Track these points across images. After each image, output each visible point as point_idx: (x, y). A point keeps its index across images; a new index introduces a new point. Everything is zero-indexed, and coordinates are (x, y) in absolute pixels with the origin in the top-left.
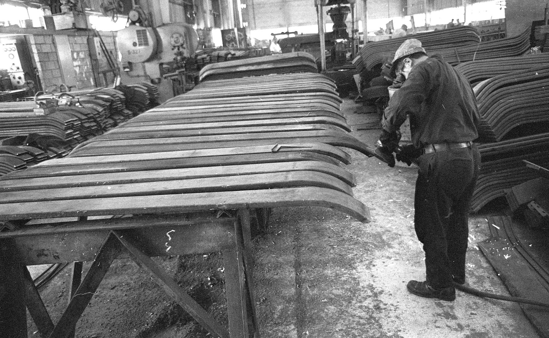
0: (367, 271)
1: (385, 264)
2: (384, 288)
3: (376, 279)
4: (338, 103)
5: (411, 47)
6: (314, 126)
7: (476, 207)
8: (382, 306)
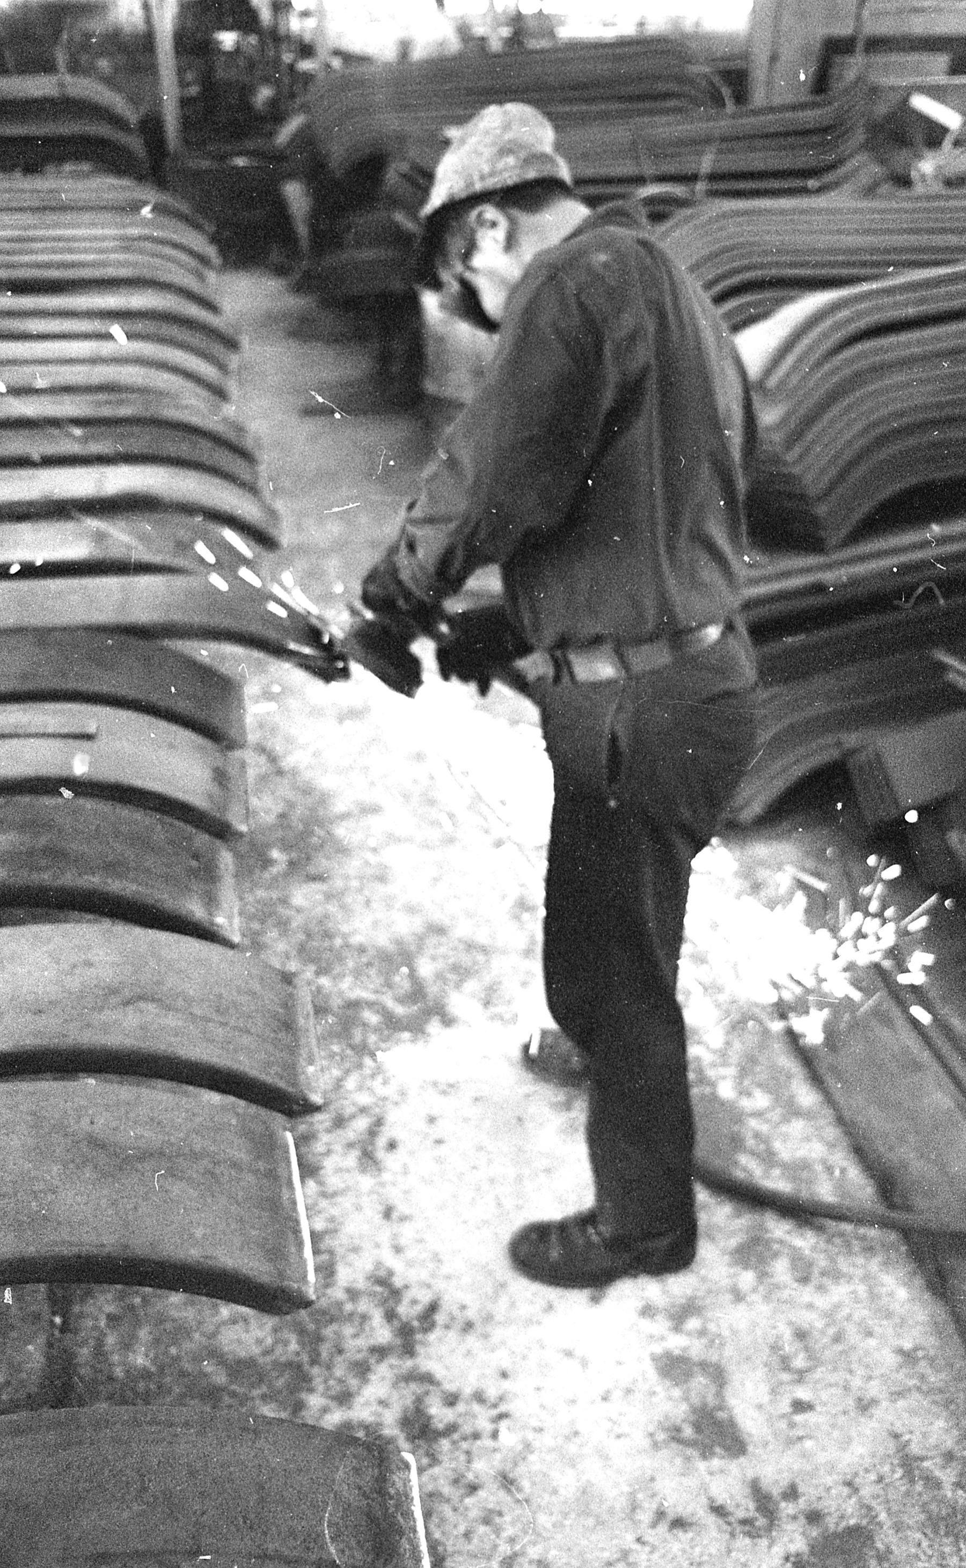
0: (366, 1182)
1: (436, 1131)
2: (440, 1285)
3: (407, 1232)
4: (217, 349)
5: (505, 151)
6: (100, 537)
7: (747, 804)
8: (439, 1413)
